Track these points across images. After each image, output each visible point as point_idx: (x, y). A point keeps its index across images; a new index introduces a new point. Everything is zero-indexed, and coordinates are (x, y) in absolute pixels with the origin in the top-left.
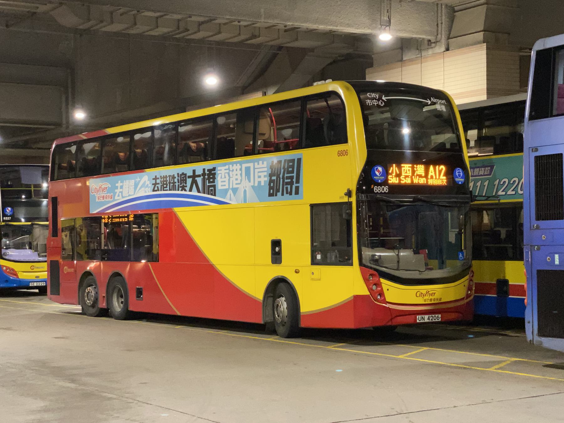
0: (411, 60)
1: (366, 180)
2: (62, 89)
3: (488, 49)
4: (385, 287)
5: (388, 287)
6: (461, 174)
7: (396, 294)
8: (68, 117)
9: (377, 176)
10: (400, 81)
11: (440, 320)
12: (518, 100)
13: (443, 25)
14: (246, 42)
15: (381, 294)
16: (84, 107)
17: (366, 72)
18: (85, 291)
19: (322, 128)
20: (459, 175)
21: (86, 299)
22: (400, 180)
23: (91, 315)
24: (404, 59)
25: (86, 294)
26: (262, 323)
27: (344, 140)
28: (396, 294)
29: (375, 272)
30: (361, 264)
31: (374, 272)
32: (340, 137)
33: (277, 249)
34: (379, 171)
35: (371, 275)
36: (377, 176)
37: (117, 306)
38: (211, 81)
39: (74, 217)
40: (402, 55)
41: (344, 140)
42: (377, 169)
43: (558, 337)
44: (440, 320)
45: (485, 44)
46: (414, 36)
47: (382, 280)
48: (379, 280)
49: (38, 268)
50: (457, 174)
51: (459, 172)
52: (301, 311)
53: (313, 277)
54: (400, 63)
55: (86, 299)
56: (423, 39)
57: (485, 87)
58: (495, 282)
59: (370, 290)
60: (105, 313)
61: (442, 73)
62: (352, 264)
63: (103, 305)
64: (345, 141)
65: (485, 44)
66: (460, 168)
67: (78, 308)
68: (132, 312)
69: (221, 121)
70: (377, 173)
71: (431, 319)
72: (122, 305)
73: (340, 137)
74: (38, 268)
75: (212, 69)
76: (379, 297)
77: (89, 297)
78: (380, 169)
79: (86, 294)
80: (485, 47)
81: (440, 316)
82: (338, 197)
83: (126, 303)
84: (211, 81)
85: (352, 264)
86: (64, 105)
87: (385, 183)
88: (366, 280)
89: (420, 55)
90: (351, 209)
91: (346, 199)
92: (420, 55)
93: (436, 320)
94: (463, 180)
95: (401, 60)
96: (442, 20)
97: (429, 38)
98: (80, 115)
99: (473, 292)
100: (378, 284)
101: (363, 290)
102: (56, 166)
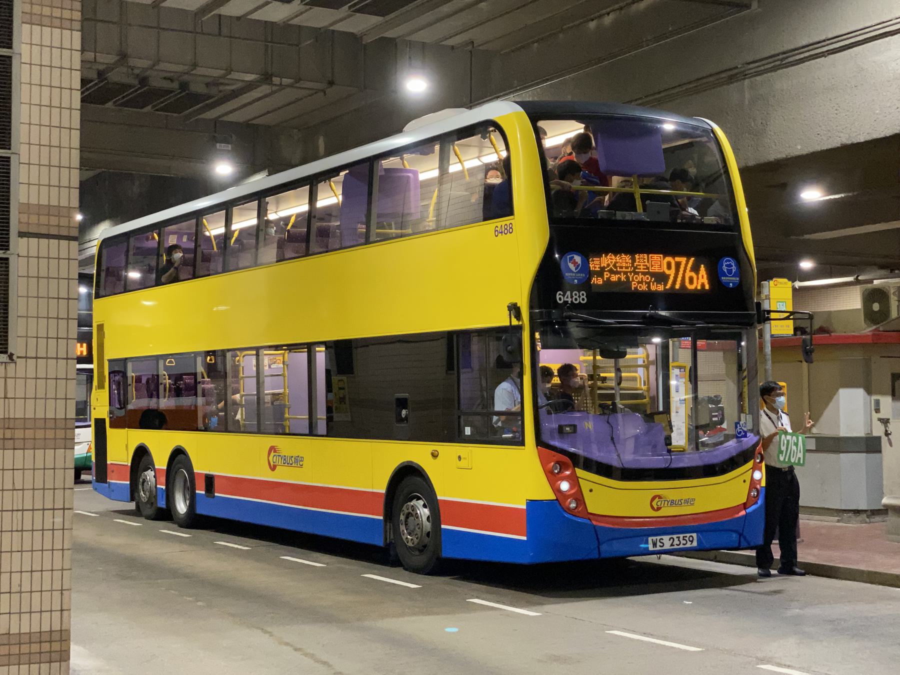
1: (547, 279)
4: (585, 486)
5: (592, 486)
7: (607, 499)
11: (695, 544)
20: (730, 272)
23: (148, 518)
25: (402, 517)
26: (380, 543)
28: (607, 499)
29: (566, 459)
31: (561, 459)
34: (575, 263)
37: (182, 507)
43: (12, 9)
44: (695, 544)
47: (580, 472)
48: (574, 473)
50: (725, 269)
51: (730, 266)
52: (108, 462)
58: (525, 507)
59: (557, 491)
60: (166, 514)
62: (522, 443)
63: (162, 504)
64: (511, 213)
66: (728, 256)
69: (823, 531)
70: (572, 266)
77: (411, 527)
82: (503, 320)
83: (191, 507)
85: (522, 443)
99: (713, 196)
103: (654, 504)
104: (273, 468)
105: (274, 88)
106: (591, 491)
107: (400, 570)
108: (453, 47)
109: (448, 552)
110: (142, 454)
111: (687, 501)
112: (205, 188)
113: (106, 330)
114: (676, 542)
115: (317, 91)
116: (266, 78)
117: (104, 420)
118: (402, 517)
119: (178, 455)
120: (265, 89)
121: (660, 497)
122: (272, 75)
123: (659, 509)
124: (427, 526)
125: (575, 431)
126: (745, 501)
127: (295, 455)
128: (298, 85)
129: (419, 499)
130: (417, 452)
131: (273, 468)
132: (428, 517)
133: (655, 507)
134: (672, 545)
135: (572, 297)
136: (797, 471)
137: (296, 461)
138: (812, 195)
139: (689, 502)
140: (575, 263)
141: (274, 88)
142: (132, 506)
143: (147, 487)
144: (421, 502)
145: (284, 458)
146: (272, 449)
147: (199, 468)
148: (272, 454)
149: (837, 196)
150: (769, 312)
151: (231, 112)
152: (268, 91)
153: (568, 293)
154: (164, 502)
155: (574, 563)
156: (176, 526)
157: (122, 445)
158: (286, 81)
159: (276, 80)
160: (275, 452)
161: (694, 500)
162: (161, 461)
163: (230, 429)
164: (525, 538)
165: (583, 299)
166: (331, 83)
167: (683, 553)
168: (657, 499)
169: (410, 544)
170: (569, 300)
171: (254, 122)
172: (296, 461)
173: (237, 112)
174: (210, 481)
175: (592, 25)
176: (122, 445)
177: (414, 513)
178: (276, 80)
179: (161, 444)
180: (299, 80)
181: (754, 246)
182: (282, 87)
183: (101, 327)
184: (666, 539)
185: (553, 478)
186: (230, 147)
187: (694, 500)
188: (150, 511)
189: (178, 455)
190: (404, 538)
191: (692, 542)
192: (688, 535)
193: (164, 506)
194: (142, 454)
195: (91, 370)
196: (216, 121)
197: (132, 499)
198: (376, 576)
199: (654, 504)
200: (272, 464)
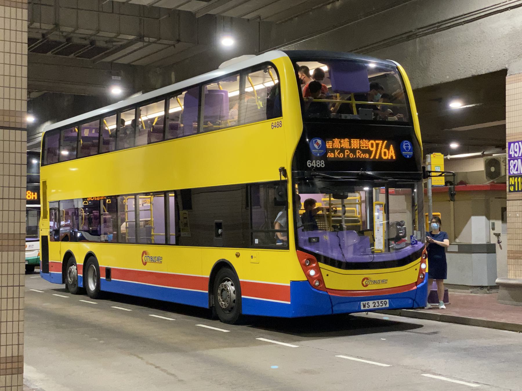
1: (302, 153)
5: (328, 272)
6: (410, 147)
7: (337, 280)
11: (388, 306)
12: (470, 129)
20: (407, 149)
23: (73, 293)
25: (219, 292)
26: (207, 306)
28: (337, 280)
30: (298, 247)
31: (310, 257)
34: (318, 144)
37: (92, 287)
39: (58, 200)
42: (315, 142)
44: (388, 306)
47: (321, 265)
49: (375, 282)
50: (404, 147)
53: (253, 260)
58: (289, 285)
59: (308, 275)
60: (83, 291)
62: (287, 248)
63: (81, 285)
64: (281, 115)
66: (406, 140)
68: (103, 292)
70: (316, 146)
74: (375, 282)
77: (224, 297)
81: (387, 301)
82: (276, 177)
83: (98, 287)
85: (287, 248)
87: (324, 157)
93: (384, 306)
102: (46, 152)
103: (364, 283)
104: (145, 264)
105: (145, 44)
106: (327, 275)
107: (218, 322)
108: (248, 20)
109: (246, 311)
110: (69, 256)
111: (383, 281)
113: (47, 184)
114: (377, 304)
115: (170, 45)
116: (140, 38)
118: (219, 292)
120: (140, 44)
121: (367, 279)
122: (144, 36)
123: (367, 286)
124: (234, 296)
125: (318, 241)
127: (157, 256)
128: (159, 42)
129: (229, 281)
130: (227, 254)
131: (145, 264)
132: (234, 292)
133: (365, 284)
134: (374, 306)
135: (316, 164)
137: (158, 260)
138: (456, 105)
139: (384, 281)
140: (318, 144)
141: (145, 44)
142: (63, 286)
143: (72, 275)
144: (230, 283)
145: (151, 258)
146: (144, 253)
148: (144, 255)
150: (430, 172)
151: (119, 58)
152: (142, 46)
153: (314, 161)
154: (82, 284)
155: (318, 317)
156: (88, 298)
158: (152, 40)
159: (146, 39)
160: (146, 254)
161: (387, 280)
162: (80, 260)
163: (119, 241)
164: (289, 303)
166: (179, 41)
167: (381, 311)
168: (366, 280)
169: (224, 307)
170: (315, 165)
171: (133, 64)
172: (158, 260)
173: (124, 57)
174: (108, 271)
175: (329, 7)
177: (226, 289)
178: (146, 39)
179: (80, 250)
180: (160, 39)
182: (150, 43)
183: (44, 183)
184: (371, 303)
185: (305, 268)
186: (120, 78)
187: (387, 280)
188: (73, 289)
189: (90, 256)
190: (220, 303)
191: (386, 304)
192: (384, 301)
193: (82, 286)
194: (69, 256)
195: (39, 208)
196: (111, 63)
197: (63, 283)
198: (204, 325)
199: (364, 283)
200: (144, 261)
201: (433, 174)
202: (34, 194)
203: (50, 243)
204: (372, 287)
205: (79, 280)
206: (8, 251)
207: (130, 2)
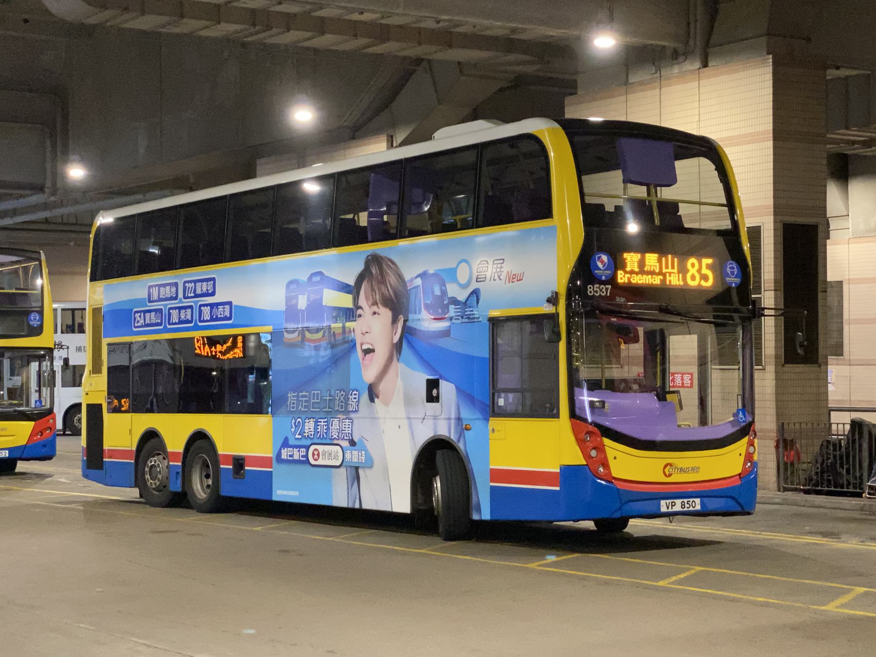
0: (641, 83)
2: (46, 130)
3: (775, 64)
7: (627, 465)
8: (55, 175)
9: (600, 269)
10: (623, 119)
13: (698, 24)
14: (365, 51)
15: (606, 465)
16: (83, 160)
17: (566, 102)
18: (145, 463)
19: (504, 191)
20: (732, 273)
21: (148, 476)
22: (684, 279)
24: (630, 81)
27: (547, 213)
30: (575, 415)
31: (594, 433)
32: (541, 208)
33: (435, 392)
34: (602, 262)
35: (588, 433)
36: (599, 269)
37: (199, 488)
38: (303, 116)
40: (627, 76)
41: (547, 213)
42: (599, 258)
45: (771, 56)
46: (650, 42)
47: (607, 441)
48: (602, 441)
49: (682, 470)
50: (32, 318)
54: (623, 89)
55: (148, 476)
56: (664, 47)
57: (770, 127)
58: (558, 471)
59: (587, 456)
60: (180, 500)
61: (696, 104)
62: (557, 416)
63: (176, 486)
65: (771, 56)
67: (134, 493)
70: (600, 265)
71: (687, 506)
72: (209, 491)
73: (541, 208)
74: (682, 470)
75: (305, 95)
76: (601, 469)
77: (154, 475)
78: (605, 258)
79: (147, 469)
80: (771, 60)
84: (303, 116)
85: (557, 416)
86: (48, 155)
87: (612, 280)
88: (580, 442)
89: (658, 75)
90: (557, 324)
91: (548, 309)
92: (658, 75)
94: (738, 280)
95: (626, 83)
96: (695, 15)
97: (676, 45)
98: (76, 173)
100: (600, 449)
101: (578, 459)
103: (666, 470)
106: (615, 458)
111: (693, 469)
112: (321, 179)
117: (99, 406)
119: (199, 440)
121: (671, 465)
123: (670, 475)
126: (740, 471)
133: (667, 473)
136: (820, 226)
139: (695, 470)
140: (602, 262)
147: (222, 449)
149: (824, 608)
150: (764, 309)
157: (122, 431)
161: (699, 468)
162: (175, 443)
165: (693, 265)
174: (239, 463)
176: (122, 431)
179: (176, 429)
181: (262, 457)
184: (678, 502)
187: (699, 468)
192: (691, 500)
199: (666, 470)
201: (766, 312)
202: (670, 281)
203: (108, 418)
204: (675, 478)
205: (173, 478)
206: (775, 290)
207: (235, 4)
